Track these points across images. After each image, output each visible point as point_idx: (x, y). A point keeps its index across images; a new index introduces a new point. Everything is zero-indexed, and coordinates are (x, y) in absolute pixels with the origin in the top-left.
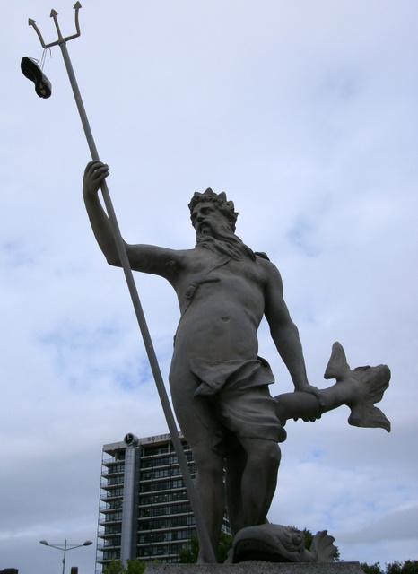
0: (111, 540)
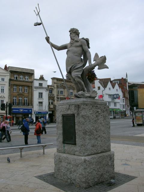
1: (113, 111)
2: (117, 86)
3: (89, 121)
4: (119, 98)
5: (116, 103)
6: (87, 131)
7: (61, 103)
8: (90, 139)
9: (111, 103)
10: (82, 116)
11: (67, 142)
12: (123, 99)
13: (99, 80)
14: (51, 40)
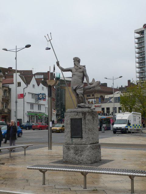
0: (140, 74)
1: (37, 117)
4: (44, 99)
5: (40, 106)
8: (91, 134)
10: (88, 120)
11: (75, 137)
13: (19, 74)
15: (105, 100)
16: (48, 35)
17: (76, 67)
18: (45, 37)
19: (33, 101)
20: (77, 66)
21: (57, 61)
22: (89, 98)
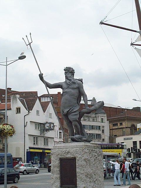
2: (50, 108)
3: (89, 164)
6: (88, 174)
7: (59, 147)
9: (39, 139)
12: (60, 132)
13: (18, 96)
14: (45, 79)
15: (138, 129)
16: (27, 36)
17: (68, 81)
18: (23, 39)
19: (37, 133)
20: (70, 80)
21: (40, 73)
22: (116, 127)
